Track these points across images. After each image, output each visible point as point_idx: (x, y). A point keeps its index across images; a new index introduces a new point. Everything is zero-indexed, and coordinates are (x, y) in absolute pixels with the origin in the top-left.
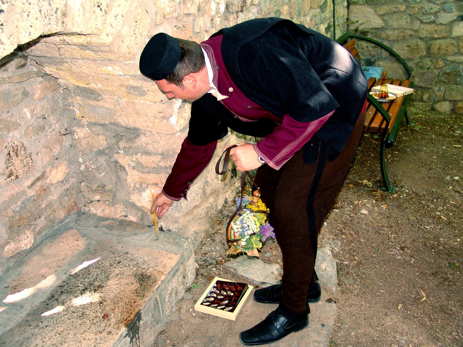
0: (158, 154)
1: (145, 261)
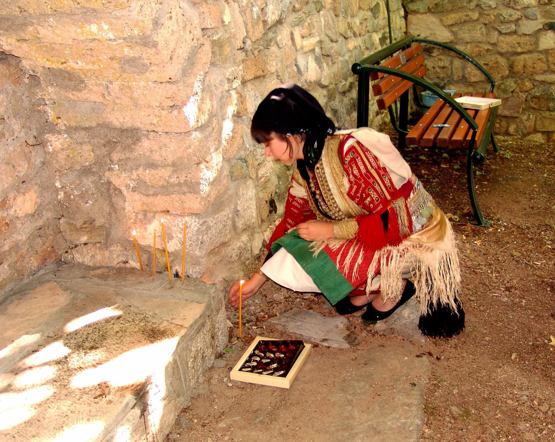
0: (168, 166)
1: (156, 314)
